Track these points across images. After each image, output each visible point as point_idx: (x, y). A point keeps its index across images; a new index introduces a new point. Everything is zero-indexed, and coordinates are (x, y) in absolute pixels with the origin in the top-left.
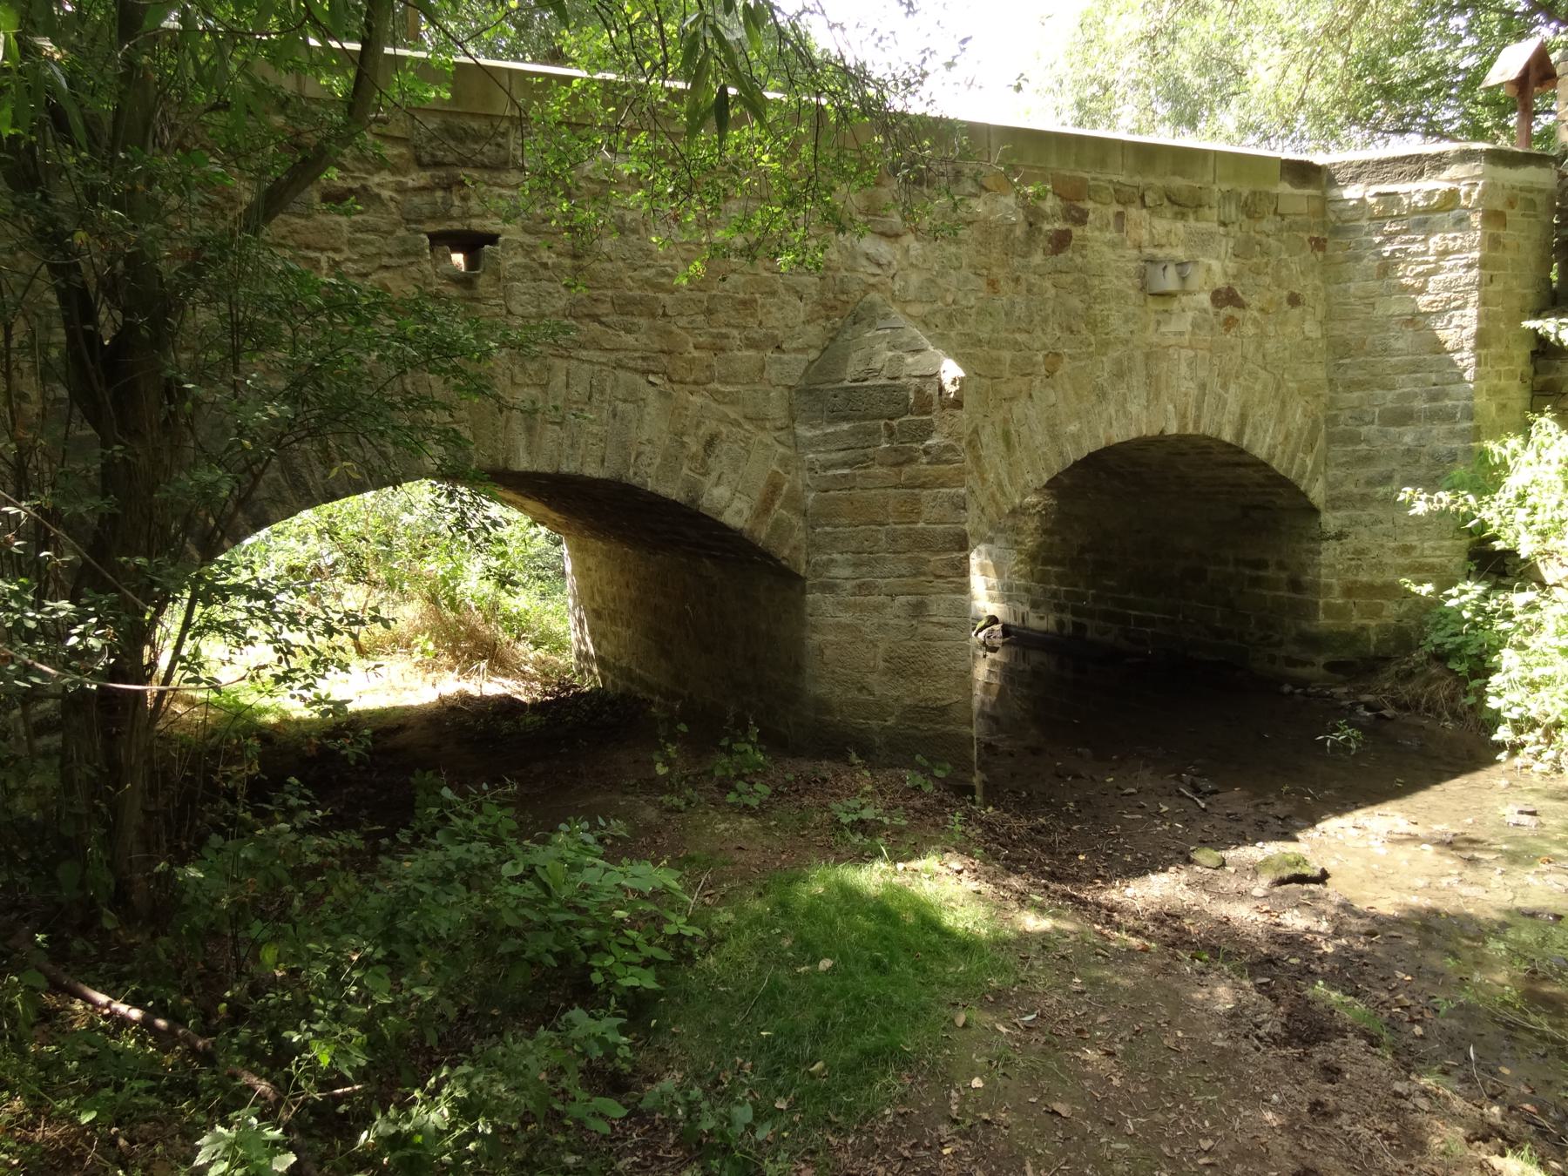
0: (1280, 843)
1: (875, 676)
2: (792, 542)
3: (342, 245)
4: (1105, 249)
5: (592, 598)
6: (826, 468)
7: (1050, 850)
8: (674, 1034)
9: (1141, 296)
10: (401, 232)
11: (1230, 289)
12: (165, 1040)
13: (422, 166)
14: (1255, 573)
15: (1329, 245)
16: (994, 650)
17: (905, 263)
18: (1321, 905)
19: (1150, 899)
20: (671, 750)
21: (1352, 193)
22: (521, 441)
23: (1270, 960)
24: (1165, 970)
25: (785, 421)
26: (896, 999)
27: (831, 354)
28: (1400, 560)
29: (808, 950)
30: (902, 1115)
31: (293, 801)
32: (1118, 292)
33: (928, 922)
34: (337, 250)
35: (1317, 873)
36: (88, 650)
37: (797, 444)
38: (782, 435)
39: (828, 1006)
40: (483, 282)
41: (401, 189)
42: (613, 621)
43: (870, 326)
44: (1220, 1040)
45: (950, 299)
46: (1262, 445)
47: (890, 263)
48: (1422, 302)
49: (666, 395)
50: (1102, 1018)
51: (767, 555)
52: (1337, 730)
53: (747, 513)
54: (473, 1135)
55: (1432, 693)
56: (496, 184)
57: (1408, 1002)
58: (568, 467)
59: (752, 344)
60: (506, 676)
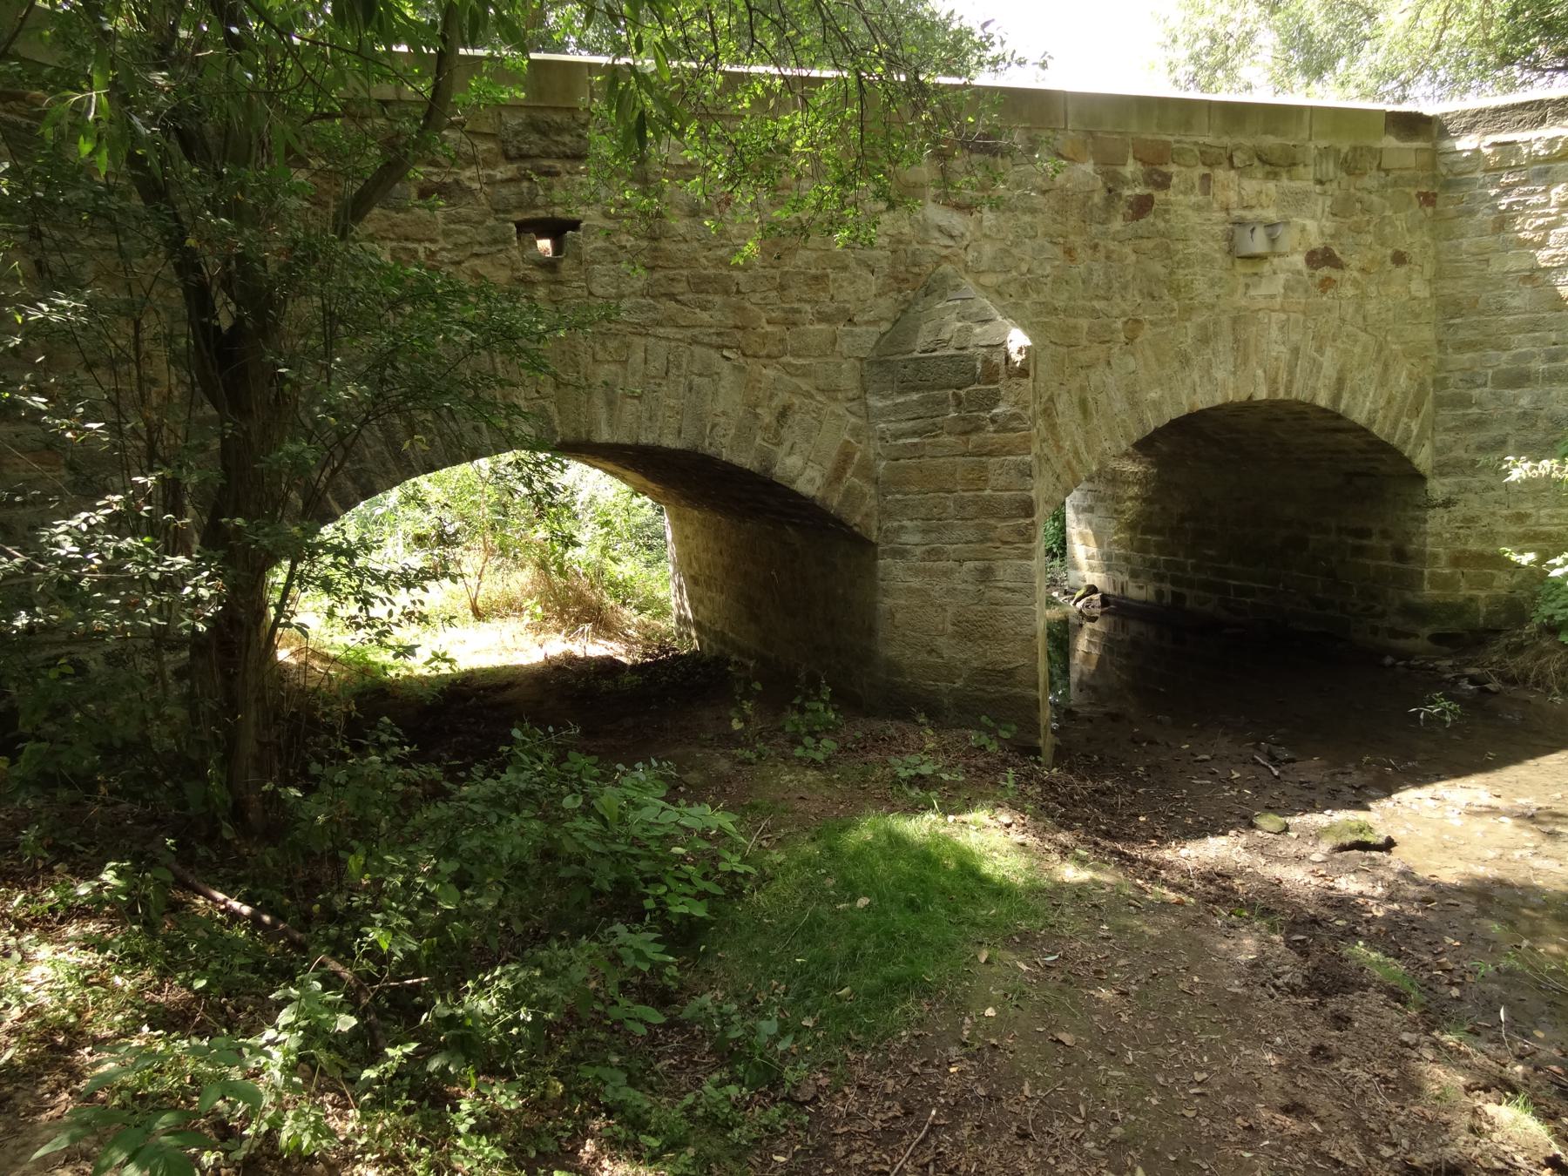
0: (1350, 812)
2: (864, 509)
3: (432, 236)
4: (1190, 212)
5: (690, 565)
6: (896, 437)
7: (1111, 811)
8: (720, 959)
9: (1229, 260)
10: (490, 222)
11: (1327, 249)
12: (271, 932)
13: (509, 159)
14: (1358, 542)
15: (1440, 201)
16: (1093, 619)
17: (978, 234)
18: (1380, 872)
19: (1202, 858)
20: (747, 706)
21: (1465, 144)
22: (603, 415)
23: (1314, 921)
24: (1194, 923)
26: (924, 936)
27: (902, 325)
28: (1513, 529)
29: (850, 889)
30: (917, 1037)
31: (385, 738)
32: (1204, 255)
33: (968, 870)
34: (433, 241)
35: (1381, 841)
36: (199, 599)
37: (868, 413)
38: (854, 406)
39: (861, 938)
40: (566, 264)
41: (491, 182)
42: (709, 587)
43: (941, 297)
44: (1236, 987)
45: (1024, 268)
46: (1363, 407)
48: (1542, 256)
49: (741, 369)
50: (1122, 962)
51: (839, 522)
52: (1433, 702)
53: (819, 481)
54: (516, 1022)
55: (1541, 667)
57: (1451, 966)
58: (646, 439)
59: (824, 318)
60: (610, 639)
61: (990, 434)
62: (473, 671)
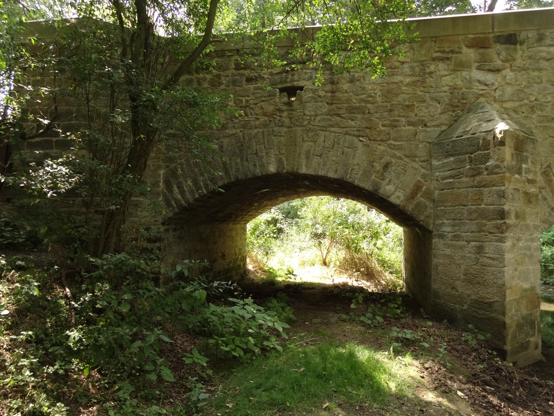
1: (459, 282)
2: (426, 214)
6: (443, 179)
17: (503, 83)
22: (304, 162)
25: (426, 158)
34: (248, 96)
38: (424, 164)
45: (533, 98)
47: (493, 84)
53: (402, 198)
56: (305, 69)
58: (321, 173)
59: (410, 124)
61: (485, 176)
62: (305, 283)
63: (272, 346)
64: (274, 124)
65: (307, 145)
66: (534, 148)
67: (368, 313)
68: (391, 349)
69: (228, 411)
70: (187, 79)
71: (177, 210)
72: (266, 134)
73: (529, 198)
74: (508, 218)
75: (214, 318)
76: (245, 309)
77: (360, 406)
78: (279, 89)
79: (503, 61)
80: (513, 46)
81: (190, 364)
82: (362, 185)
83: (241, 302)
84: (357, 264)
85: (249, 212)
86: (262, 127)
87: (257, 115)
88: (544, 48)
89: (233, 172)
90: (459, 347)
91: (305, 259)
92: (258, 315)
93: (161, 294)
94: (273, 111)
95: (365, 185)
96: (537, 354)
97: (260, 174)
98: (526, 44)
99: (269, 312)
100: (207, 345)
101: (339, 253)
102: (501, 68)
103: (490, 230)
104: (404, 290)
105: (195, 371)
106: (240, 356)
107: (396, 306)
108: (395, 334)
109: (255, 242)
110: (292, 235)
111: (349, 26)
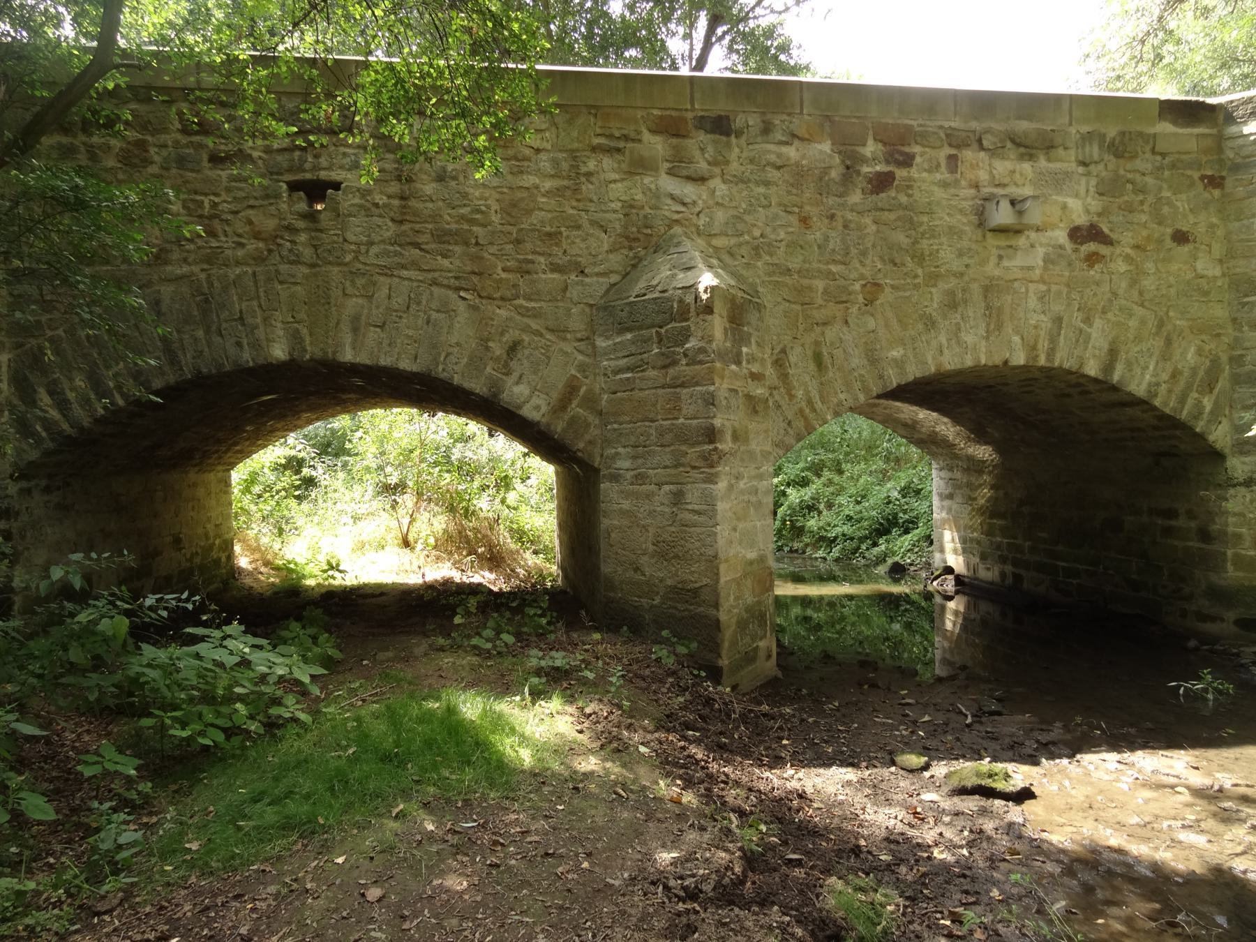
1: (645, 558)
2: (587, 437)
17: (711, 202)
22: (348, 338)
34: (215, 194)
38: (582, 345)
45: (757, 233)
46: (1140, 378)
47: (694, 203)
53: (544, 409)
58: (385, 361)
59: (556, 268)
61: (683, 368)
62: (365, 585)
63: (288, 715)
64: (278, 258)
65: (353, 305)
66: (761, 319)
67: (486, 628)
68: (526, 689)
69: (188, 857)
70: (60, 146)
71: (50, 445)
72: (261, 278)
73: (754, 406)
74: (720, 441)
75: (153, 674)
76: (225, 647)
77: (465, 801)
78: (288, 183)
79: (709, 164)
80: (724, 138)
81: (95, 776)
82: (467, 385)
83: (217, 634)
84: (468, 540)
85: (236, 444)
86: (252, 262)
87: (240, 236)
88: (771, 147)
89: (187, 360)
90: (647, 672)
91: (365, 538)
92: (256, 657)
93: (14, 634)
94: (275, 230)
95: (473, 385)
96: (768, 667)
97: (251, 364)
98: (744, 137)
99: (281, 649)
100: (139, 732)
101: (435, 521)
102: (707, 175)
103: (693, 464)
104: (560, 582)
105: (110, 791)
106: (216, 745)
107: (539, 612)
108: (534, 662)
109: (253, 508)
110: (335, 491)
111: (426, 68)
